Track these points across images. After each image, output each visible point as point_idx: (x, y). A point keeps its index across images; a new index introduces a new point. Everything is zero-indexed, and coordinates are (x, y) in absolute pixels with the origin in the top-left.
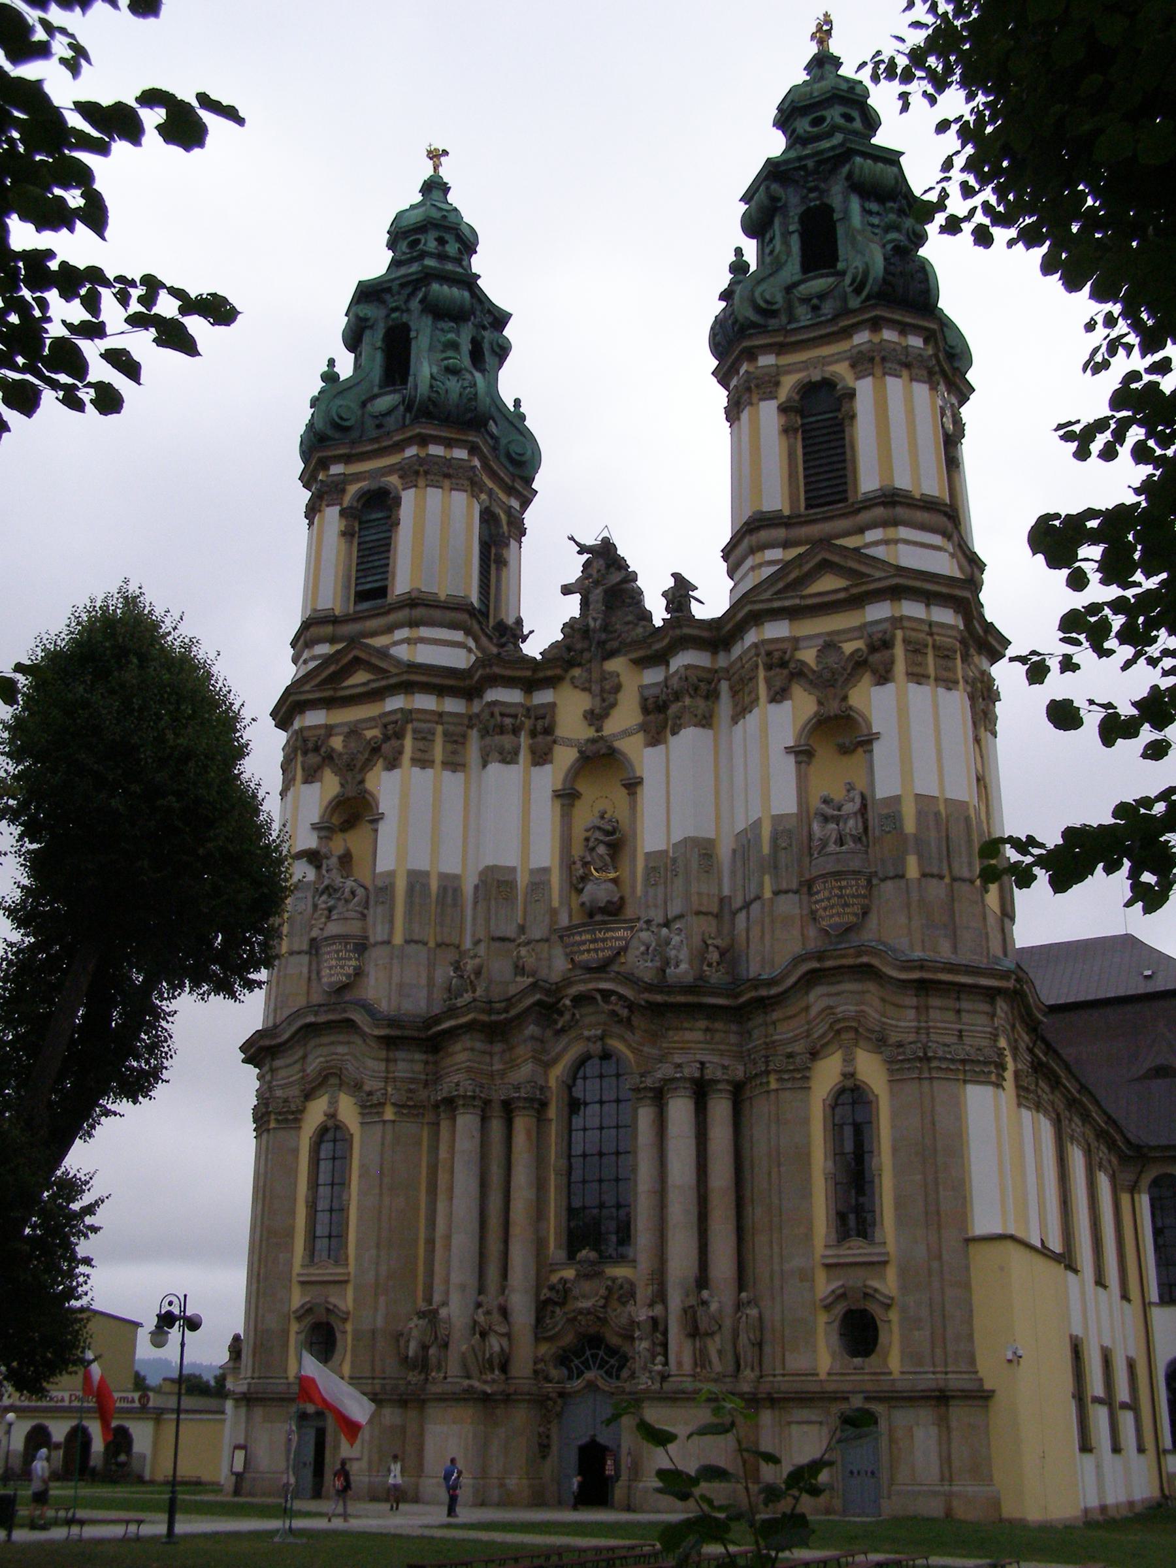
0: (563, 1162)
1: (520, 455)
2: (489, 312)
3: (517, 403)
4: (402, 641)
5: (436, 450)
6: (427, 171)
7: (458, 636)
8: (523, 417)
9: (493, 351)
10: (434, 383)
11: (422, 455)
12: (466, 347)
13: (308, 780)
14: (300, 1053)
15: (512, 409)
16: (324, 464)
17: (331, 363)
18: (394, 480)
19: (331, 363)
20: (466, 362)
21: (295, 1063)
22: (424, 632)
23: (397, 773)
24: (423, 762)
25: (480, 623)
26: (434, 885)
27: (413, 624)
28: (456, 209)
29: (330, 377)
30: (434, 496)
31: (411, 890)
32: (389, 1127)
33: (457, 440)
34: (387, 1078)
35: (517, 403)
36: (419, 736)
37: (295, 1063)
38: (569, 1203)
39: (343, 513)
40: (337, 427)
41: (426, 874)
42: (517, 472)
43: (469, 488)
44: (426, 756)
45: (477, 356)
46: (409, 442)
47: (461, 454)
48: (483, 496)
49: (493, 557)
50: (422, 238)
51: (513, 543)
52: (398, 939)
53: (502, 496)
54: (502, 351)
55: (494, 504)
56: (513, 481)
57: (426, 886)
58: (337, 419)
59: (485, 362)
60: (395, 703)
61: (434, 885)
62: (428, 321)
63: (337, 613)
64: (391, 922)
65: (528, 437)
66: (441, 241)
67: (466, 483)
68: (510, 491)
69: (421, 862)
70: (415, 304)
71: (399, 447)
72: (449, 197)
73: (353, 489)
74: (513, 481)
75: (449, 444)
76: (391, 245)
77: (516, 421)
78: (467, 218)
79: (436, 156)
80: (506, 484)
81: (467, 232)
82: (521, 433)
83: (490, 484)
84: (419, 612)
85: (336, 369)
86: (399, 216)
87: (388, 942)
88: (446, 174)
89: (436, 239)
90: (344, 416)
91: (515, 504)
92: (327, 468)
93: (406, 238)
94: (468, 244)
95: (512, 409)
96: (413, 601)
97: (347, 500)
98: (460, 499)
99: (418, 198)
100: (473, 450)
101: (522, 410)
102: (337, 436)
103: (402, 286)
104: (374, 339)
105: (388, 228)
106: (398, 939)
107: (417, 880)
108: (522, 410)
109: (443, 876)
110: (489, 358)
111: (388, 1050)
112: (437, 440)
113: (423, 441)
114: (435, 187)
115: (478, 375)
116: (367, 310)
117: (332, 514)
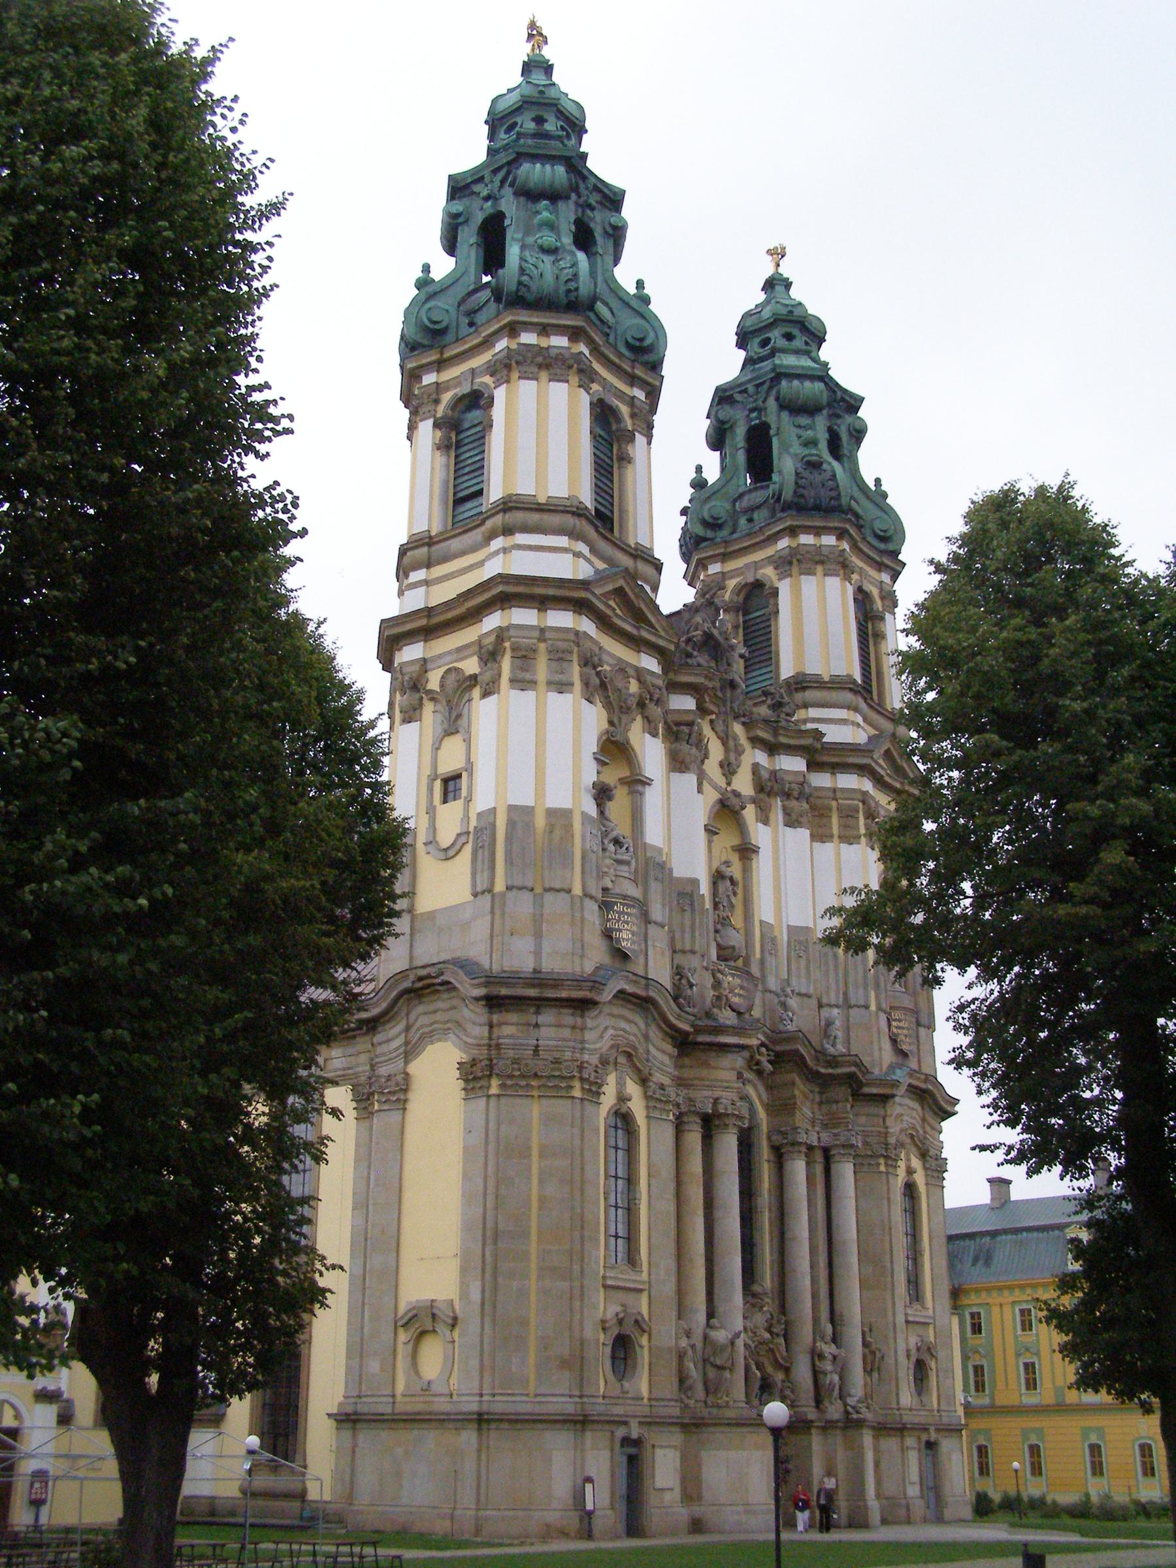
0: (892, 1196)
1: (885, 531)
2: (596, 189)
3: (878, 482)
4: (497, 553)
5: (806, 539)
6: (769, 271)
7: (563, 541)
8: (885, 496)
9: (606, 234)
10: (524, 265)
11: (514, 346)
12: (823, 437)
13: (407, 720)
14: (401, 1026)
15: (873, 488)
16: (702, 564)
17: (699, 469)
18: (769, 572)
19: (699, 469)
20: (567, 240)
21: (400, 1034)
22: (521, 538)
23: (493, 700)
24: (521, 683)
25: (865, 699)
26: (540, 822)
27: (508, 531)
28: (800, 304)
29: (699, 484)
30: (809, 584)
31: (511, 824)
32: (493, 1101)
33: (824, 528)
34: (490, 1046)
35: (878, 482)
36: (520, 654)
37: (400, 1034)
38: (404, 1114)
39: (436, 425)
40: (706, 524)
41: (528, 811)
42: (882, 546)
43: (841, 572)
44: (528, 676)
45: (584, 238)
46: (496, 334)
47: (829, 540)
48: (595, 387)
49: (870, 632)
50: (519, 120)
51: (888, 616)
52: (499, 886)
53: (872, 572)
54: (858, 434)
55: (865, 582)
56: (633, 368)
57: (529, 826)
58: (428, 324)
59: (595, 243)
60: (492, 621)
61: (540, 822)
62: (785, 415)
63: (433, 534)
64: (492, 868)
65: (889, 512)
66: (539, 120)
67: (838, 567)
68: (880, 567)
69: (523, 796)
70: (772, 403)
71: (487, 343)
72: (791, 292)
73: (447, 397)
74: (633, 368)
75: (818, 532)
76: (741, 343)
77: (878, 500)
78: (812, 310)
79: (778, 254)
80: (626, 373)
81: (815, 323)
82: (882, 510)
83: (860, 564)
84: (518, 517)
85: (431, 275)
86: (747, 315)
87: (490, 890)
88: (787, 269)
89: (533, 120)
90: (435, 319)
91: (886, 577)
92: (705, 568)
93: (502, 125)
94: (575, 125)
95: (873, 488)
96: (508, 505)
97: (441, 410)
98: (834, 584)
99: (761, 297)
100: (841, 534)
101: (883, 488)
102: (709, 534)
103: (495, 172)
104: (469, 237)
105: (485, 117)
106: (499, 886)
107: (520, 816)
108: (883, 488)
109: (552, 813)
110: (602, 243)
111: (491, 1013)
112: (807, 530)
113: (793, 532)
114: (537, 66)
115: (581, 256)
116: (726, 412)
117: (426, 427)
